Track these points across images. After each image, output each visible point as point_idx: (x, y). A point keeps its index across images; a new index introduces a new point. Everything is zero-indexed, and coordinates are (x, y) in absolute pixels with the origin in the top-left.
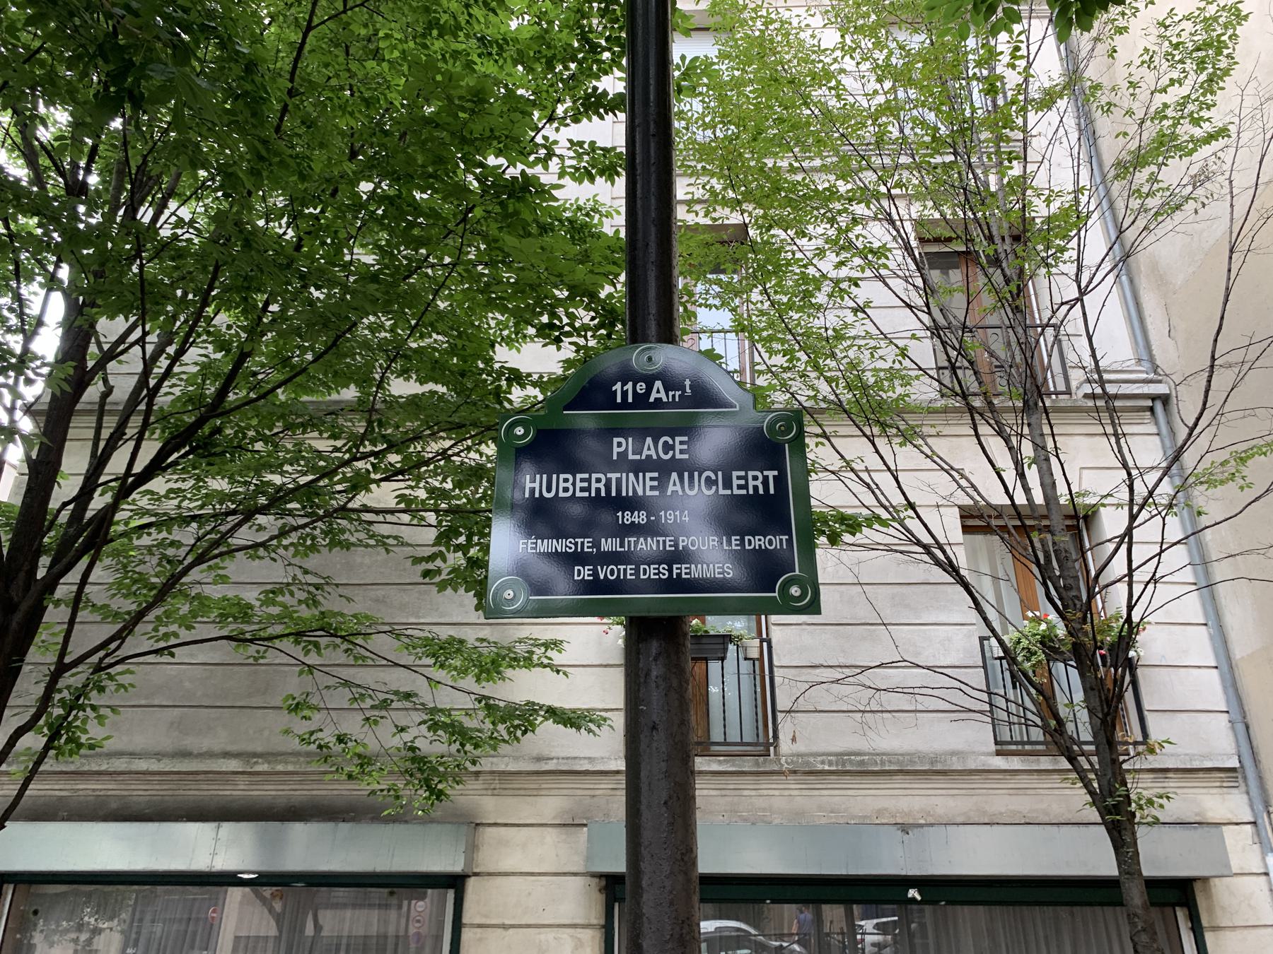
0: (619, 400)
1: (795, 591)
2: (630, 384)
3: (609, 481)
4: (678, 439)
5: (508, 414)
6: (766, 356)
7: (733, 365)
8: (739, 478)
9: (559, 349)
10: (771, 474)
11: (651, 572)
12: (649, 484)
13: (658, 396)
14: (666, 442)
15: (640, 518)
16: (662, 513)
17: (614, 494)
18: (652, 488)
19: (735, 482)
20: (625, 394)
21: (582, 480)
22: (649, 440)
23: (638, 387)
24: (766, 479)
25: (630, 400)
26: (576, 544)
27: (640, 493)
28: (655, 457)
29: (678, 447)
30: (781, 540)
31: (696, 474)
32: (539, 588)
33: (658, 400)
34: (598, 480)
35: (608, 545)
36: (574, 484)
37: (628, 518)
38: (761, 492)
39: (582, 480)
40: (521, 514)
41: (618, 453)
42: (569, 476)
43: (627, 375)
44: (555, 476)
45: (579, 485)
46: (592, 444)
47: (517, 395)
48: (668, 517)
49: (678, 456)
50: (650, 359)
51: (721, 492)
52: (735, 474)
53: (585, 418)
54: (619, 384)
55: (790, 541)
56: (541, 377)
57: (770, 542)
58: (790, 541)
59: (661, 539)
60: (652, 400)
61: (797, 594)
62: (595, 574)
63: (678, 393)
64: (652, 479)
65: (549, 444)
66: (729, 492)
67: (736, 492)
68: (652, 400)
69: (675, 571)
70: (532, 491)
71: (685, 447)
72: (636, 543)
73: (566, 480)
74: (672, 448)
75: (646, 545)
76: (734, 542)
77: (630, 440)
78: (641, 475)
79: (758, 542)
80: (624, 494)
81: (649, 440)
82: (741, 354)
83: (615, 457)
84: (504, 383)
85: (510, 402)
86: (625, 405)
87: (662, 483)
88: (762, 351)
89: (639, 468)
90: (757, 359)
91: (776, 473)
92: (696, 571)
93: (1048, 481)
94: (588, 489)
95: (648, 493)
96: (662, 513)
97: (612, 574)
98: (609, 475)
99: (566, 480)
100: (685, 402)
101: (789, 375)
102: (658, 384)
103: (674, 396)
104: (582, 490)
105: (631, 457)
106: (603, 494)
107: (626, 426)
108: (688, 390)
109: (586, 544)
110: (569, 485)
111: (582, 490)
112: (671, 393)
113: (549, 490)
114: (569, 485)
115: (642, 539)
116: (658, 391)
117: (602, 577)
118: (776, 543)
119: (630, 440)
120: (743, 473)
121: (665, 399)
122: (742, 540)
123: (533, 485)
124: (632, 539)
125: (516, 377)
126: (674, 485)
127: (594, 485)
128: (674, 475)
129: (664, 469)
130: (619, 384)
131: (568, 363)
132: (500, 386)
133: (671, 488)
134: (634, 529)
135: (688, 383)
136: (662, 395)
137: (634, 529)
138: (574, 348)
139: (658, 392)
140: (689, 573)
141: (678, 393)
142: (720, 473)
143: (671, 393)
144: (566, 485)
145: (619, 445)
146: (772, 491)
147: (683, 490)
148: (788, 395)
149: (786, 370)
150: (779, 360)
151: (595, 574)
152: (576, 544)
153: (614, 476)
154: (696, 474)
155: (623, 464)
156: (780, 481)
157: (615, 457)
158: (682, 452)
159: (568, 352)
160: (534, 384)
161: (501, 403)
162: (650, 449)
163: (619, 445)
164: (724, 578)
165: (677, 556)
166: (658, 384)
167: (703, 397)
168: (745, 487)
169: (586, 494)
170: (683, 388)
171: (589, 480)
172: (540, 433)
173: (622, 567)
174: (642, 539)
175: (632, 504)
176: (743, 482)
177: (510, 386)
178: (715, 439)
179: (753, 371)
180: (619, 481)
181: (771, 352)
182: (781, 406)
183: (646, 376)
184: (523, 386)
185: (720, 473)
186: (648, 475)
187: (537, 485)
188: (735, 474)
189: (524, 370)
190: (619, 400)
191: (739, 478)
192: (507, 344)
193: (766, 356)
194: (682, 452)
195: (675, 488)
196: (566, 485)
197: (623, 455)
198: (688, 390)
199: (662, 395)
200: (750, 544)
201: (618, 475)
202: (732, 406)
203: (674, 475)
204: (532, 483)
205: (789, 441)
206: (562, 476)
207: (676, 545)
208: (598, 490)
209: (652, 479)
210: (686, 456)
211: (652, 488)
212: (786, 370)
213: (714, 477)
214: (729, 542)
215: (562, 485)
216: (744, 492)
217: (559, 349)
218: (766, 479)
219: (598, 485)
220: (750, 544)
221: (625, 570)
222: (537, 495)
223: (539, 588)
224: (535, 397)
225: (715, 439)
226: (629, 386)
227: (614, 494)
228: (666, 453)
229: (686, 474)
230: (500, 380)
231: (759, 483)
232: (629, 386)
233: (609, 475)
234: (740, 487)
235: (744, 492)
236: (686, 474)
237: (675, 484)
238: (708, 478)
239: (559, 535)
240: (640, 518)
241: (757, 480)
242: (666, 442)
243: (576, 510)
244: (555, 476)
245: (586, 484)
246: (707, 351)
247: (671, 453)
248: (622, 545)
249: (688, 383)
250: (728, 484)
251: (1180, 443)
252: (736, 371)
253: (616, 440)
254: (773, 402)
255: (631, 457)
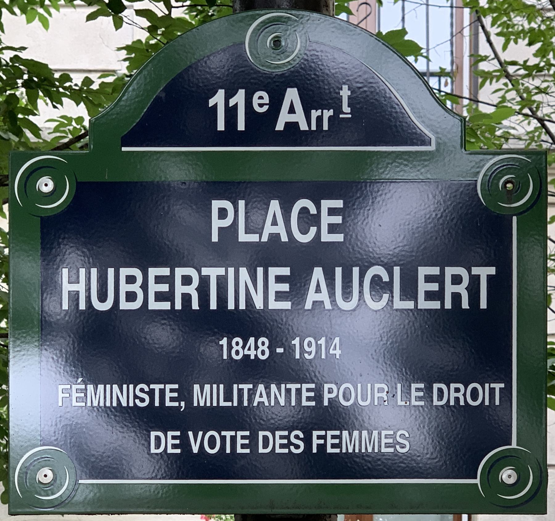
0: (221, 126)
1: (508, 475)
2: (241, 93)
3: (204, 282)
4: (326, 204)
5: (33, 151)
6: (498, 42)
7: (440, 59)
8: (429, 279)
9: (118, 24)
10: (485, 272)
11: (273, 443)
12: (274, 287)
13: (292, 118)
14: (304, 211)
15: (259, 349)
16: (296, 342)
17: (213, 306)
18: (280, 296)
19: (423, 287)
20: (231, 113)
21: (159, 280)
22: (275, 206)
23: (256, 101)
24: (475, 280)
25: (241, 126)
26: (151, 393)
27: (259, 304)
28: (284, 238)
29: (326, 220)
30: (492, 391)
31: (356, 271)
32: (97, 465)
33: (292, 126)
34: (457, 280)
35: (206, 395)
36: (145, 287)
37: (237, 349)
38: (465, 305)
39: (159, 280)
40: (65, 342)
41: (221, 230)
42: (136, 272)
43: (245, 78)
44: (111, 272)
45: (153, 288)
46: (184, 214)
47: (48, 117)
48: (306, 348)
49: (326, 237)
50: (277, 42)
51: (399, 304)
52: (423, 271)
53: (171, 162)
54: (221, 93)
55: (506, 393)
56: (88, 82)
57: (474, 394)
58: (506, 393)
59: (293, 387)
60: (280, 126)
61: (512, 481)
62: (184, 444)
63: (328, 114)
64: (279, 279)
65: (104, 210)
66: (410, 305)
67: (424, 304)
68: (280, 126)
69: (316, 442)
70: (74, 297)
71: (338, 220)
72: (252, 393)
73: (131, 280)
74: (316, 220)
75: (270, 397)
76: (414, 394)
77: (242, 204)
78: (260, 271)
79: (455, 393)
80: (231, 306)
81: (275, 206)
82: (456, 35)
83: (215, 238)
84: (21, 92)
85: (35, 130)
86: (231, 136)
87: (298, 285)
88: (493, 31)
89: (264, 256)
90: (484, 49)
91: (492, 271)
92: (351, 442)
93: (237, 289)
94: (168, 296)
95: (273, 305)
96: (296, 342)
97: (212, 444)
98: (205, 271)
99: (131, 280)
100: (338, 131)
101: (537, 82)
102: (292, 95)
103: (320, 119)
104: (160, 297)
105: (243, 237)
106: (195, 306)
107: (247, 178)
108: (346, 108)
109: (168, 393)
110: (136, 288)
111: (160, 297)
112: (315, 114)
113: (103, 298)
114: (136, 288)
115: (261, 387)
116: (292, 111)
117: (195, 450)
118: (484, 397)
119: (242, 204)
120: (435, 271)
121: (304, 127)
122: (429, 390)
123: (74, 287)
124: (246, 387)
125: (44, 81)
126: (317, 293)
127: (180, 289)
128: (318, 273)
129: (300, 261)
130: (221, 93)
131: (133, 49)
132: (14, 99)
133: (312, 296)
134: (250, 370)
135: (345, 93)
136: (299, 117)
137: (250, 370)
138: (146, 23)
139: (292, 110)
140: (338, 446)
141: (328, 114)
142: (397, 270)
143: (315, 114)
144: (131, 288)
145: (223, 213)
146: (483, 305)
147: (333, 301)
148: (535, 123)
149: (532, 71)
150: (522, 52)
151: (184, 444)
152: (151, 393)
153: (213, 273)
154: (356, 271)
155: (227, 250)
156: (499, 285)
157: (215, 238)
158: (332, 229)
159: (135, 30)
160: (77, 96)
161: (19, 133)
162: (276, 223)
163: (223, 213)
164: (396, 454)
165: (331, 417)
166: (292, 95)
167: (376, 121)
168: (439, 295)
169: (166, 306)
170: (338, 110)
171: (170, 280)
172: (82, 189)
173: (228, 434)
174: (261, 387)
175: (247, 323)
176: (435, 287)
177: (33, 100)
178: (400, 211)
179: (475, 73)
180: (222, 282)
181: (509, 35)
182: (521, 145)
183: (269, 77)
184: (56, 99)
185: (397, 270)
186: (274, 272)
187: (81, 287)
188: (423, 271)
189: (56, 63)
190: (221, 126)
191: (429, 279)
192: (24, 11)
193: (498, 42)
194: (332, 229)
195: (318, 297)
196: (131, 288)
197: (229, 233)
198: (346, 108)
199: (299, 117)
200: (440, 397)
201: (221, 271)
202: (425, 142)
203: (318, 273)
204: (76, 284)
205: (520, 212)
206: (124, 272)
207: (318, 397)
208: (186, 298)
209: (279, 279)
210: (339, 238)
211: (280, 296)
212: (532, 71)
213: (386, 278)
214: (407, 392)
215: (124, 288)
216: (435, 305)
217: (118, 24)
218: (475, 280)
219: (187, 289)
220: (440, 397)
221: (233, 439)
222: (82, 306)
223: (97, 465)
224: (80, 120)
225: (400, 211)
226: (239, 98)
227: (213, 306)
228: (304, 232)
229: (339, 271)
230: (14, 86)
231: (192, 290)
232: (239, 98)
233: (205, 271)
234: (430, 296)
235: (435, 305)
236: (339, 271)
237: (318, 290)
238: (376, 280)
239: (130, 375)
240: (259, 349)
241: (461, 283)
242: (304, 211)
243: (162, 337)
244: (111, 272)
245: (165, 288)
246: (392, 34)
247: (313, 230)
248: (228, 397)
249: (345, 93)
250: (409, 290)
251: (365, 21)
252: (441, 74)
253: (216, 204)
254: (506, 137)
255: (243, 237)
